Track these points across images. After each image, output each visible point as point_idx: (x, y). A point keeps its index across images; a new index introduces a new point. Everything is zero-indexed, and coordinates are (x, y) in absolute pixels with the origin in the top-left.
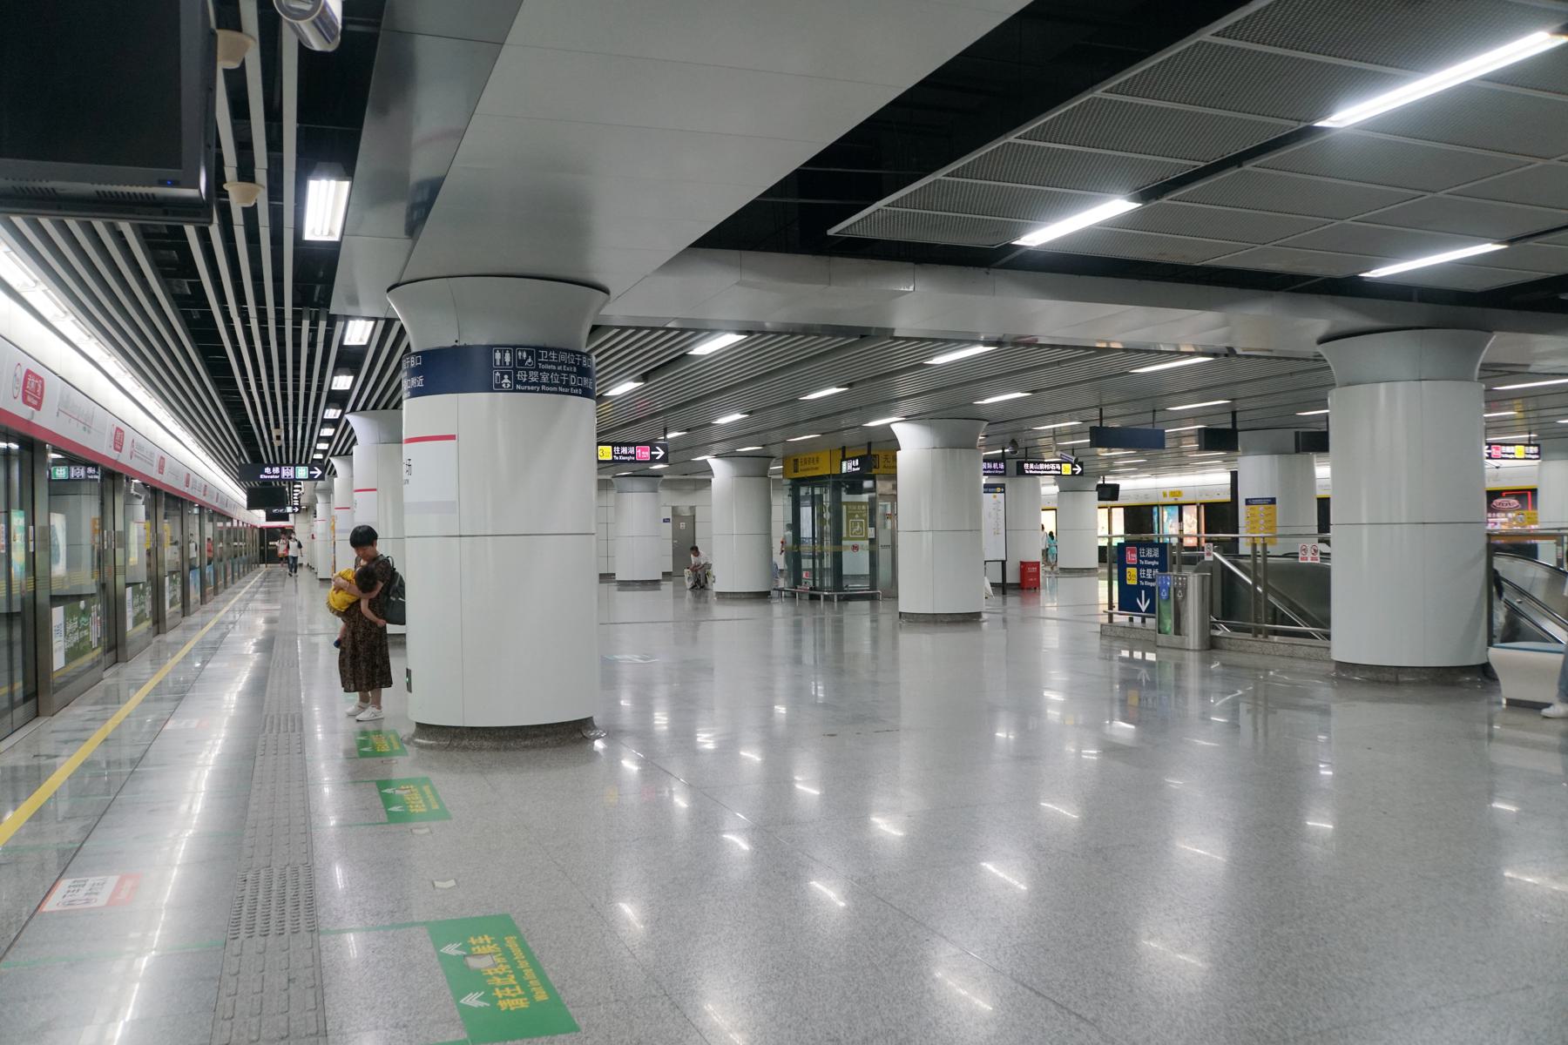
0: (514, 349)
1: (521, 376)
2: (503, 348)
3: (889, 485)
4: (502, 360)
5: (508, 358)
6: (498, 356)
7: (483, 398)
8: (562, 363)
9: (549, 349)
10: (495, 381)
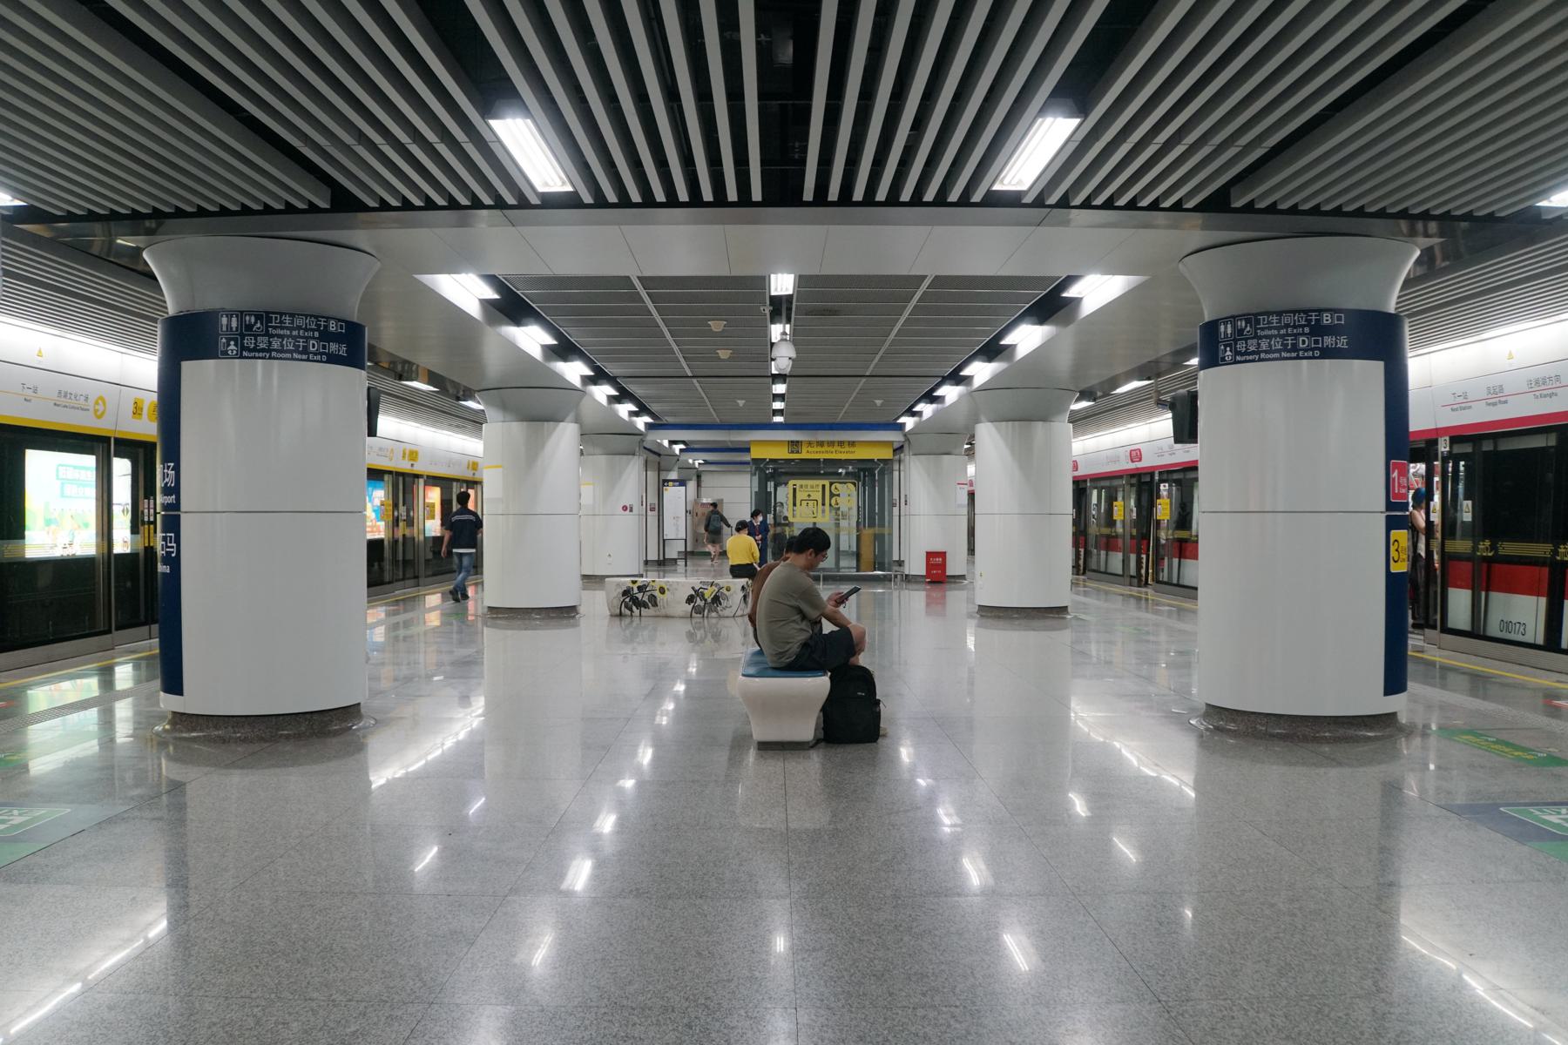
0: (241, 314)
1: (249, 342)
2: (1225, 320)
3: (1395, 569)
4: (229, 325)
5: (234, 324)
6: (224, 320)
7: (211, 362)
8: (299, 328)
9: (1268, 313)
10: (221, 348)
